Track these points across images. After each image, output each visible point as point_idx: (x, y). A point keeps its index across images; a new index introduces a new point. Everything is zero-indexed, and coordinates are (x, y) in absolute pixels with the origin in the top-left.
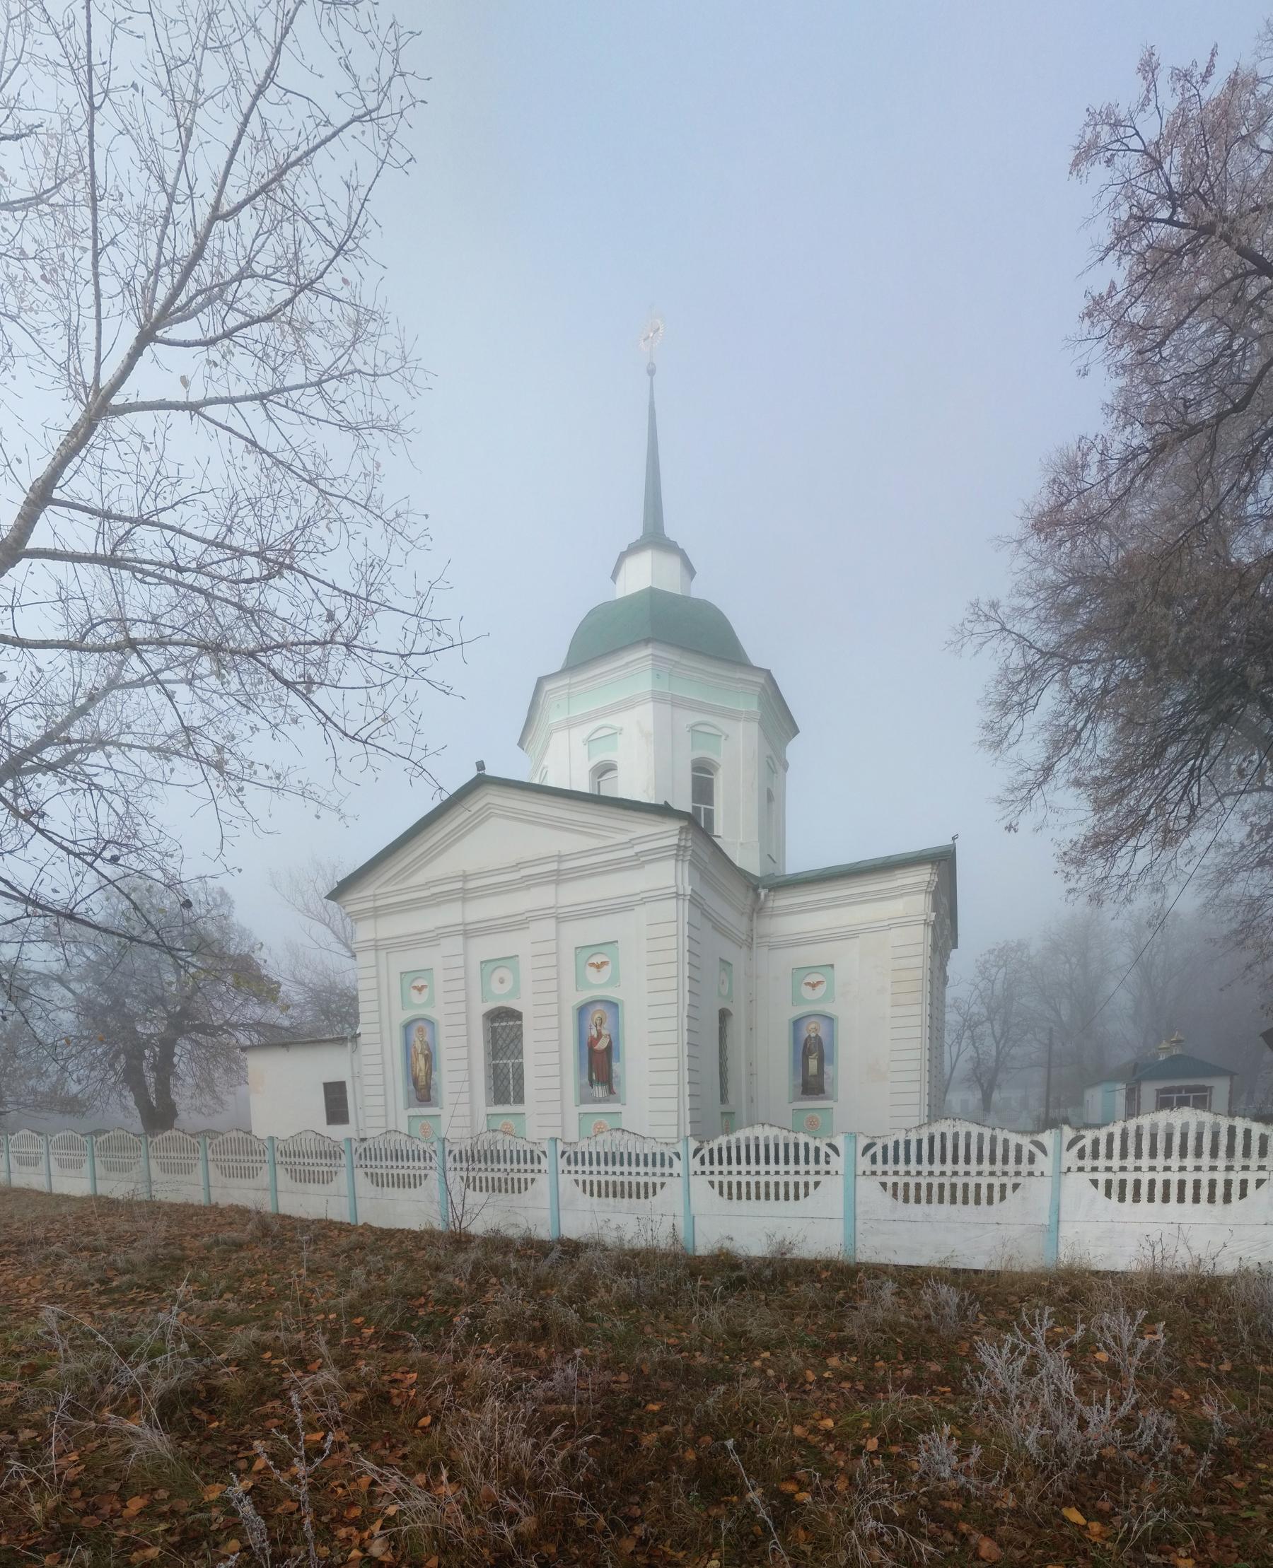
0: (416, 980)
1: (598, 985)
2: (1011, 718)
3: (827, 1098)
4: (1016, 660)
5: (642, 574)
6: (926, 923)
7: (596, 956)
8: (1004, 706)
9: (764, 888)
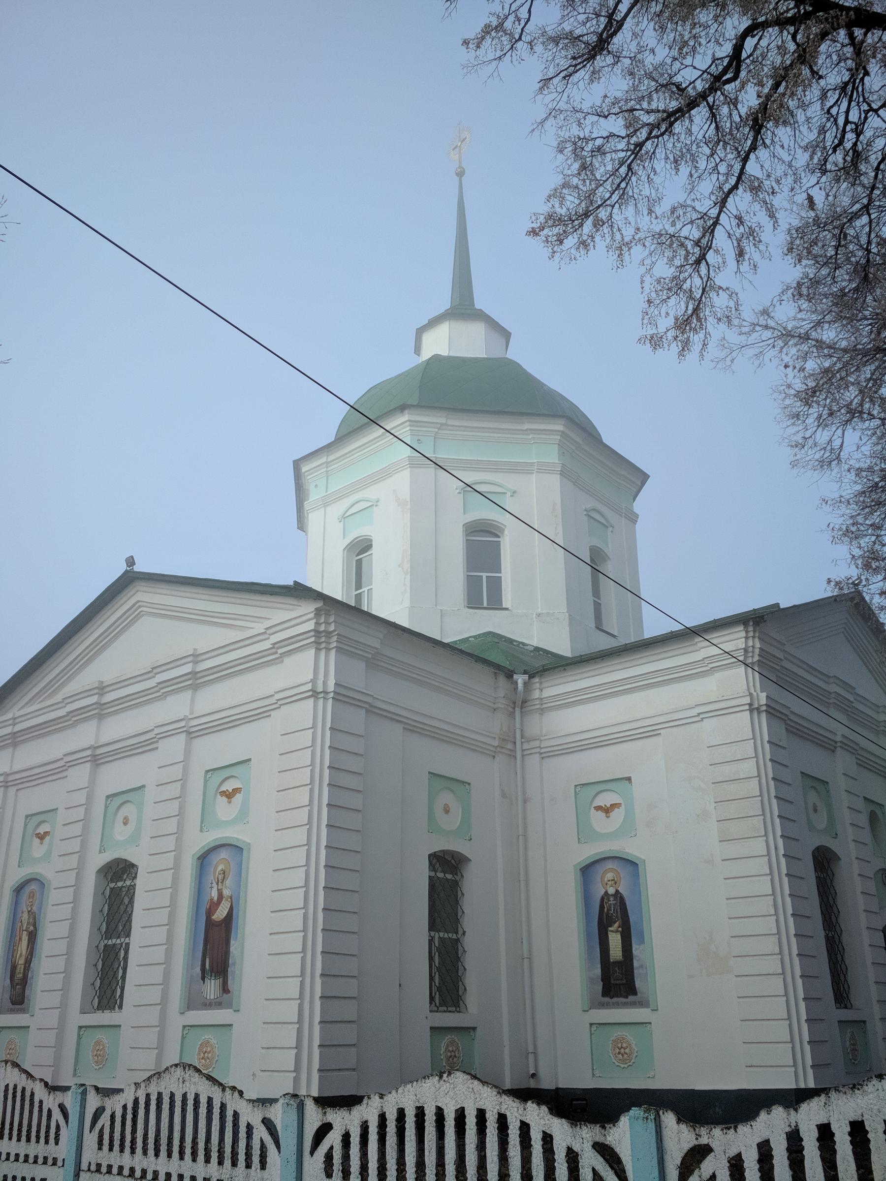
3: (643, 1004)
6: (752, 709)
7: (226, 782)
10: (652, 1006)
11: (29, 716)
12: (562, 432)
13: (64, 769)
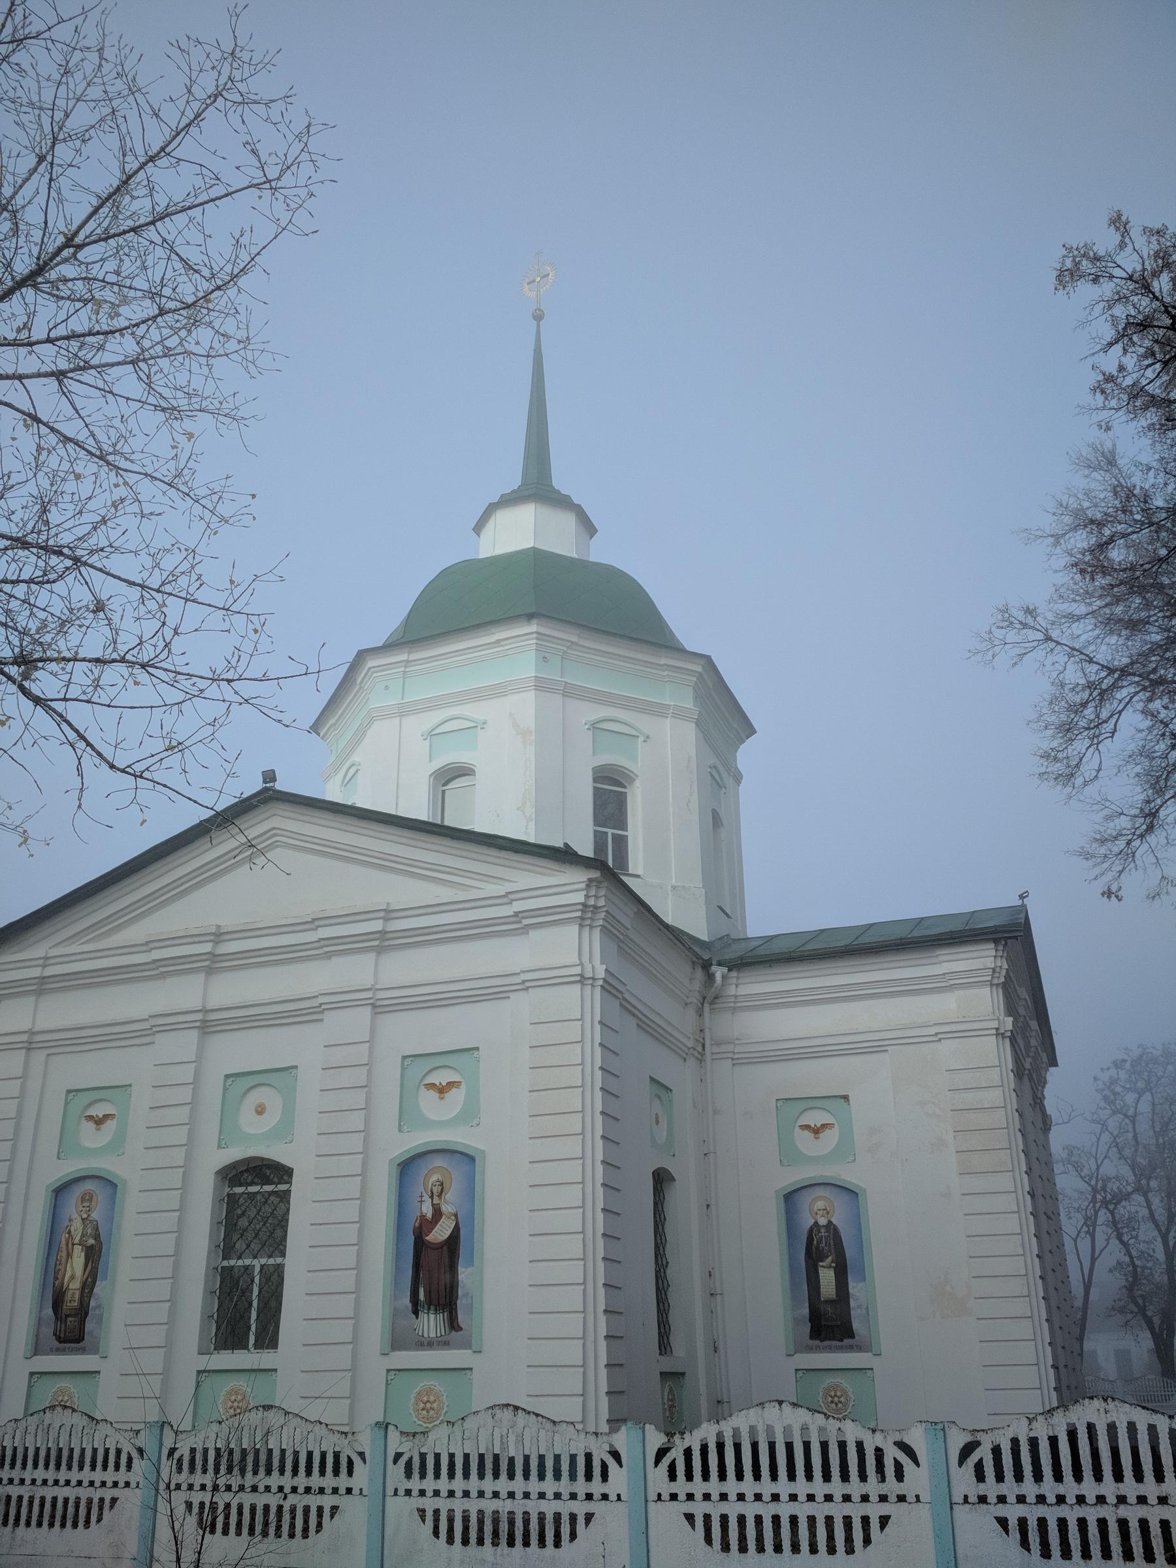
0: (94, 1107)
1: (440, 1121)
2: (1080, 745)
4: (1073, 675)
5: (516, 532)
6: (999, 1034)
8: (1067, 730)
9: (719, 962)
10: (475, 1348)
11: (73, 958)
12: (700, 673)
13: (154, 1031)
